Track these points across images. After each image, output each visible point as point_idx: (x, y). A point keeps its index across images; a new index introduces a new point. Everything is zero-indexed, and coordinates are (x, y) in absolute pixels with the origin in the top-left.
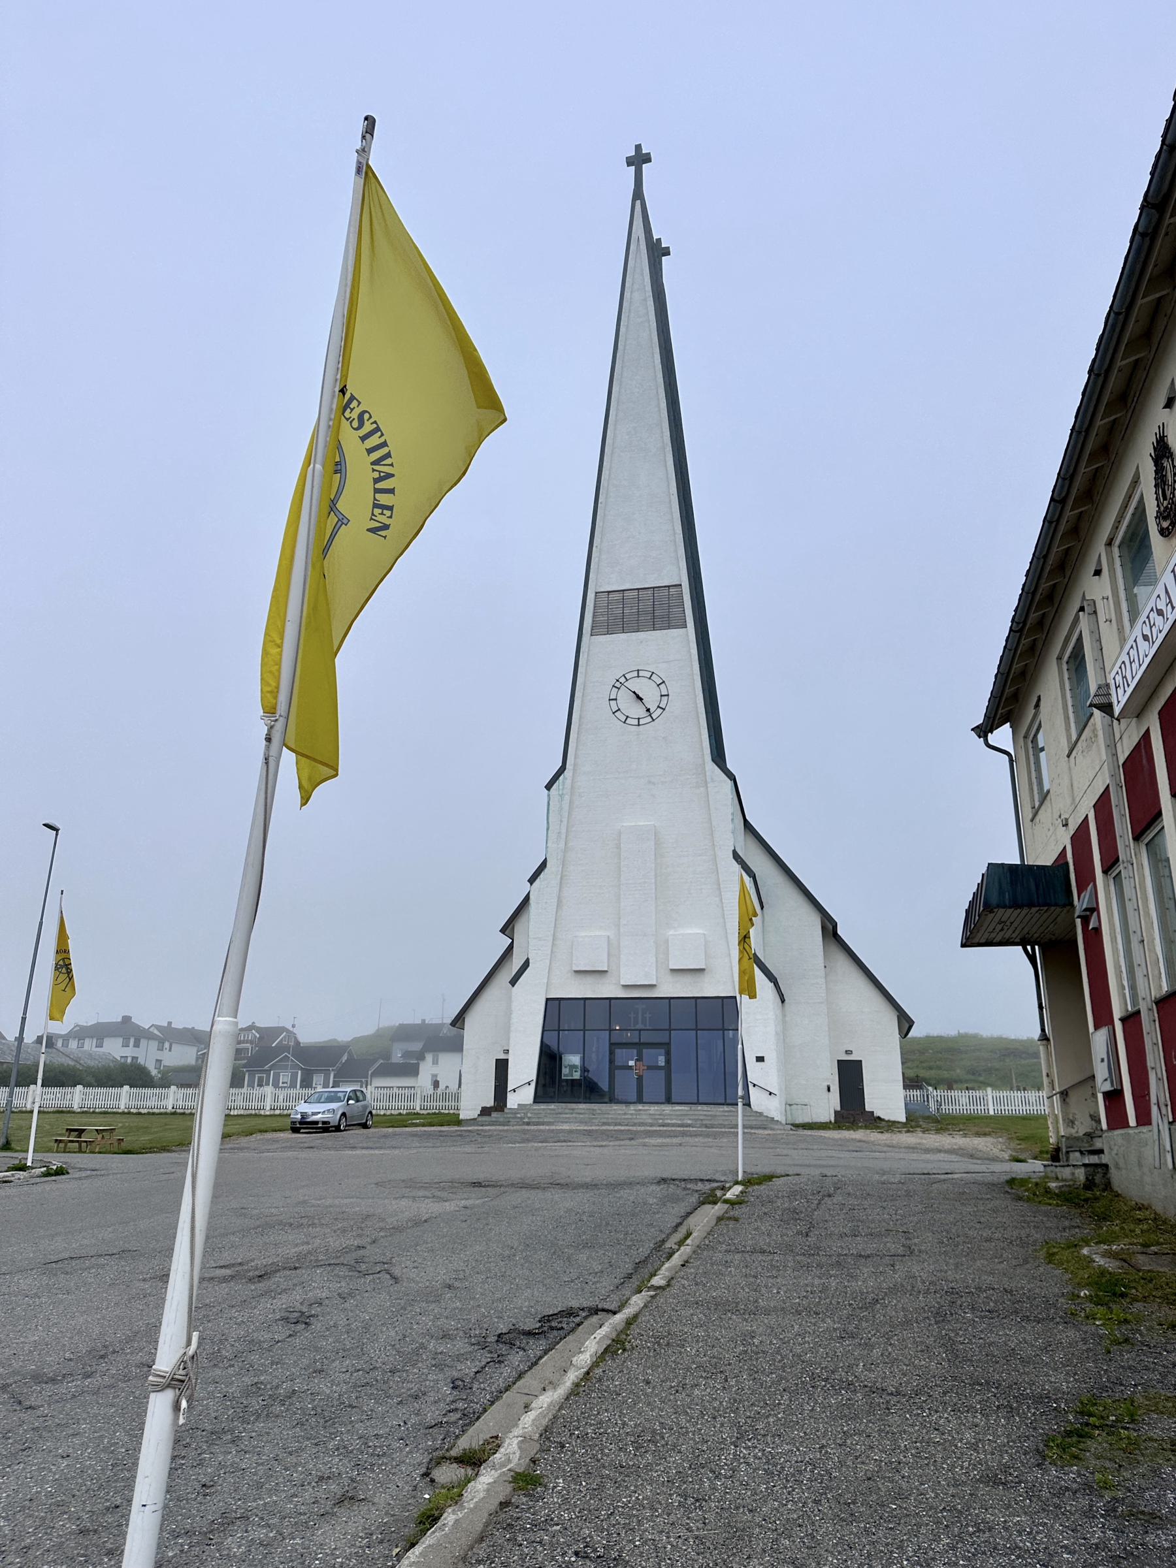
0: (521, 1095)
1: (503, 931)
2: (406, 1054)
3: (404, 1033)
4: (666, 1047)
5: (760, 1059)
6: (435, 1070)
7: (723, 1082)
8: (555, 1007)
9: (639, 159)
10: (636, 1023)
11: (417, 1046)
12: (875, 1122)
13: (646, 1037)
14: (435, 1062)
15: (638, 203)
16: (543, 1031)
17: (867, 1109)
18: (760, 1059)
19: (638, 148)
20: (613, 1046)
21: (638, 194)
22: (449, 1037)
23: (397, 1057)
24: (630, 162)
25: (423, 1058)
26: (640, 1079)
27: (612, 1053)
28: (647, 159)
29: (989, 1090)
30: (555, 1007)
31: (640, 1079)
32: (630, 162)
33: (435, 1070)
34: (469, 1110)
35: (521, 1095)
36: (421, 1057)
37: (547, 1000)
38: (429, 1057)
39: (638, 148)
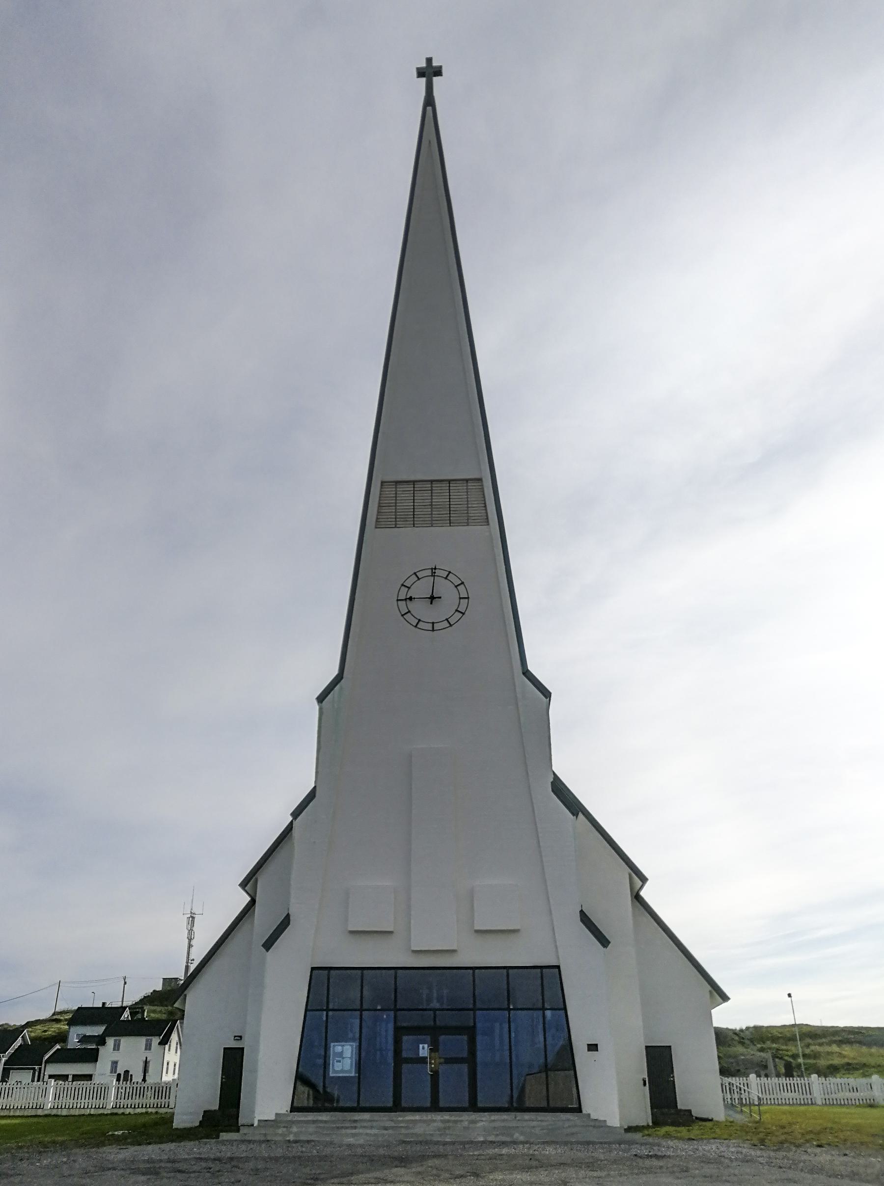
0: (270, 1096)
1: (244, 885)
2: (84, 1039)
3: (82, 1016)
4: (471, 1032)
5: (593, 1047)
6: (115, 1056)
7: (550, 1081)
8: (323, 979)
9: (430, 72)
10: (429, 1000)
11: (98, 1030)
12: (686, 1119)
13: (444, 1019)
14: (117, 1047)
15: (429, 109)
16: (306, 1010)
17: (680, 1106)
18: (593, 1047)
19: (429, 60)
20: (399, 1032)
21: (430, 101)
22: (157, 1015)
23: (73, 1042)
24: (421, 73)
25: (103, 1043)
26: (435, 1076)
27: (397, 1042)
28: (438, 72)
29: (814, 1076)
30: (323, 979)
31: (435, 1076)
32: (421, 73)
33: (115, 1056)
34: (186, 1115)
35: (270, 1096)
36: (101, 1040)
37: (313, 969)
38: (110, 1042)
39: (429, 60)
